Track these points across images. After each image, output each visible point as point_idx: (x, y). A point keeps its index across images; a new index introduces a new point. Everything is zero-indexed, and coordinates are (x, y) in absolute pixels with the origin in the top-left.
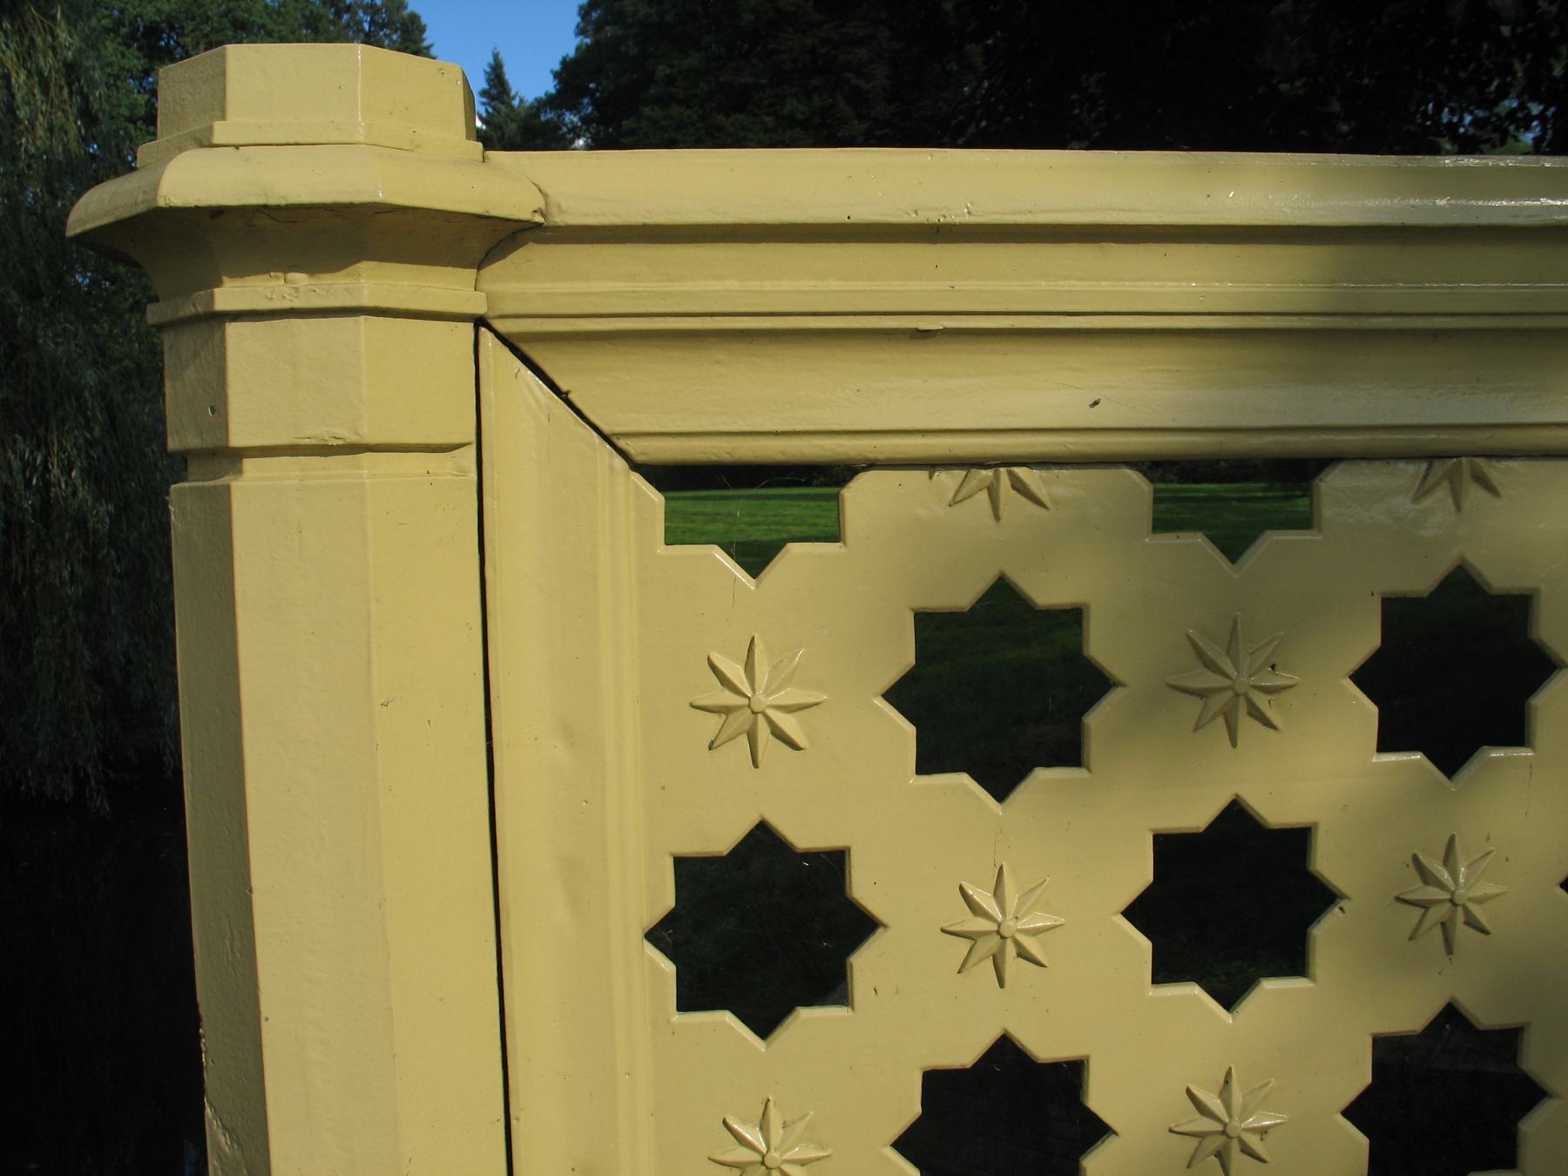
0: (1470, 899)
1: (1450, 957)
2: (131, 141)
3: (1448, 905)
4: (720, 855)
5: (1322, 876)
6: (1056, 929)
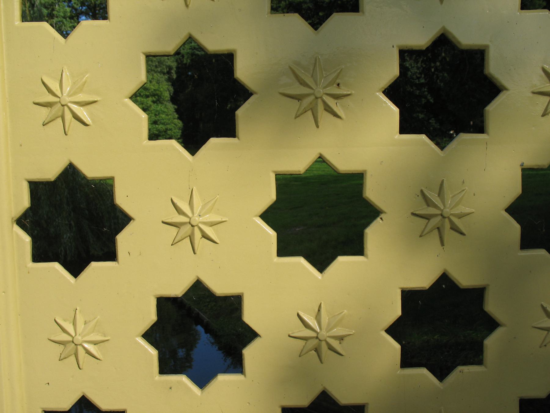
0: (451, 214)
1: (443, 247)
2: (65, 26)
3: (440, 217)
4: (49, 180)
5: (370, 200)
6: (223, 223)
